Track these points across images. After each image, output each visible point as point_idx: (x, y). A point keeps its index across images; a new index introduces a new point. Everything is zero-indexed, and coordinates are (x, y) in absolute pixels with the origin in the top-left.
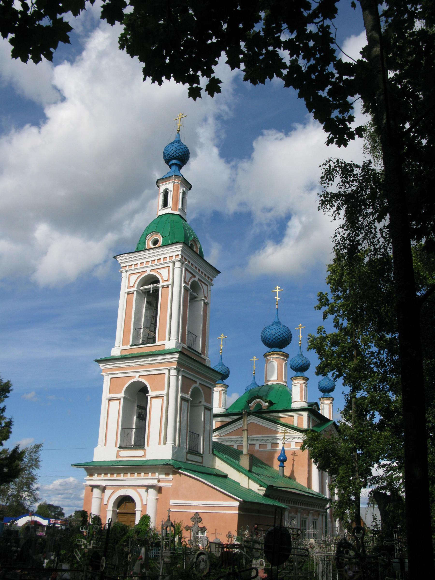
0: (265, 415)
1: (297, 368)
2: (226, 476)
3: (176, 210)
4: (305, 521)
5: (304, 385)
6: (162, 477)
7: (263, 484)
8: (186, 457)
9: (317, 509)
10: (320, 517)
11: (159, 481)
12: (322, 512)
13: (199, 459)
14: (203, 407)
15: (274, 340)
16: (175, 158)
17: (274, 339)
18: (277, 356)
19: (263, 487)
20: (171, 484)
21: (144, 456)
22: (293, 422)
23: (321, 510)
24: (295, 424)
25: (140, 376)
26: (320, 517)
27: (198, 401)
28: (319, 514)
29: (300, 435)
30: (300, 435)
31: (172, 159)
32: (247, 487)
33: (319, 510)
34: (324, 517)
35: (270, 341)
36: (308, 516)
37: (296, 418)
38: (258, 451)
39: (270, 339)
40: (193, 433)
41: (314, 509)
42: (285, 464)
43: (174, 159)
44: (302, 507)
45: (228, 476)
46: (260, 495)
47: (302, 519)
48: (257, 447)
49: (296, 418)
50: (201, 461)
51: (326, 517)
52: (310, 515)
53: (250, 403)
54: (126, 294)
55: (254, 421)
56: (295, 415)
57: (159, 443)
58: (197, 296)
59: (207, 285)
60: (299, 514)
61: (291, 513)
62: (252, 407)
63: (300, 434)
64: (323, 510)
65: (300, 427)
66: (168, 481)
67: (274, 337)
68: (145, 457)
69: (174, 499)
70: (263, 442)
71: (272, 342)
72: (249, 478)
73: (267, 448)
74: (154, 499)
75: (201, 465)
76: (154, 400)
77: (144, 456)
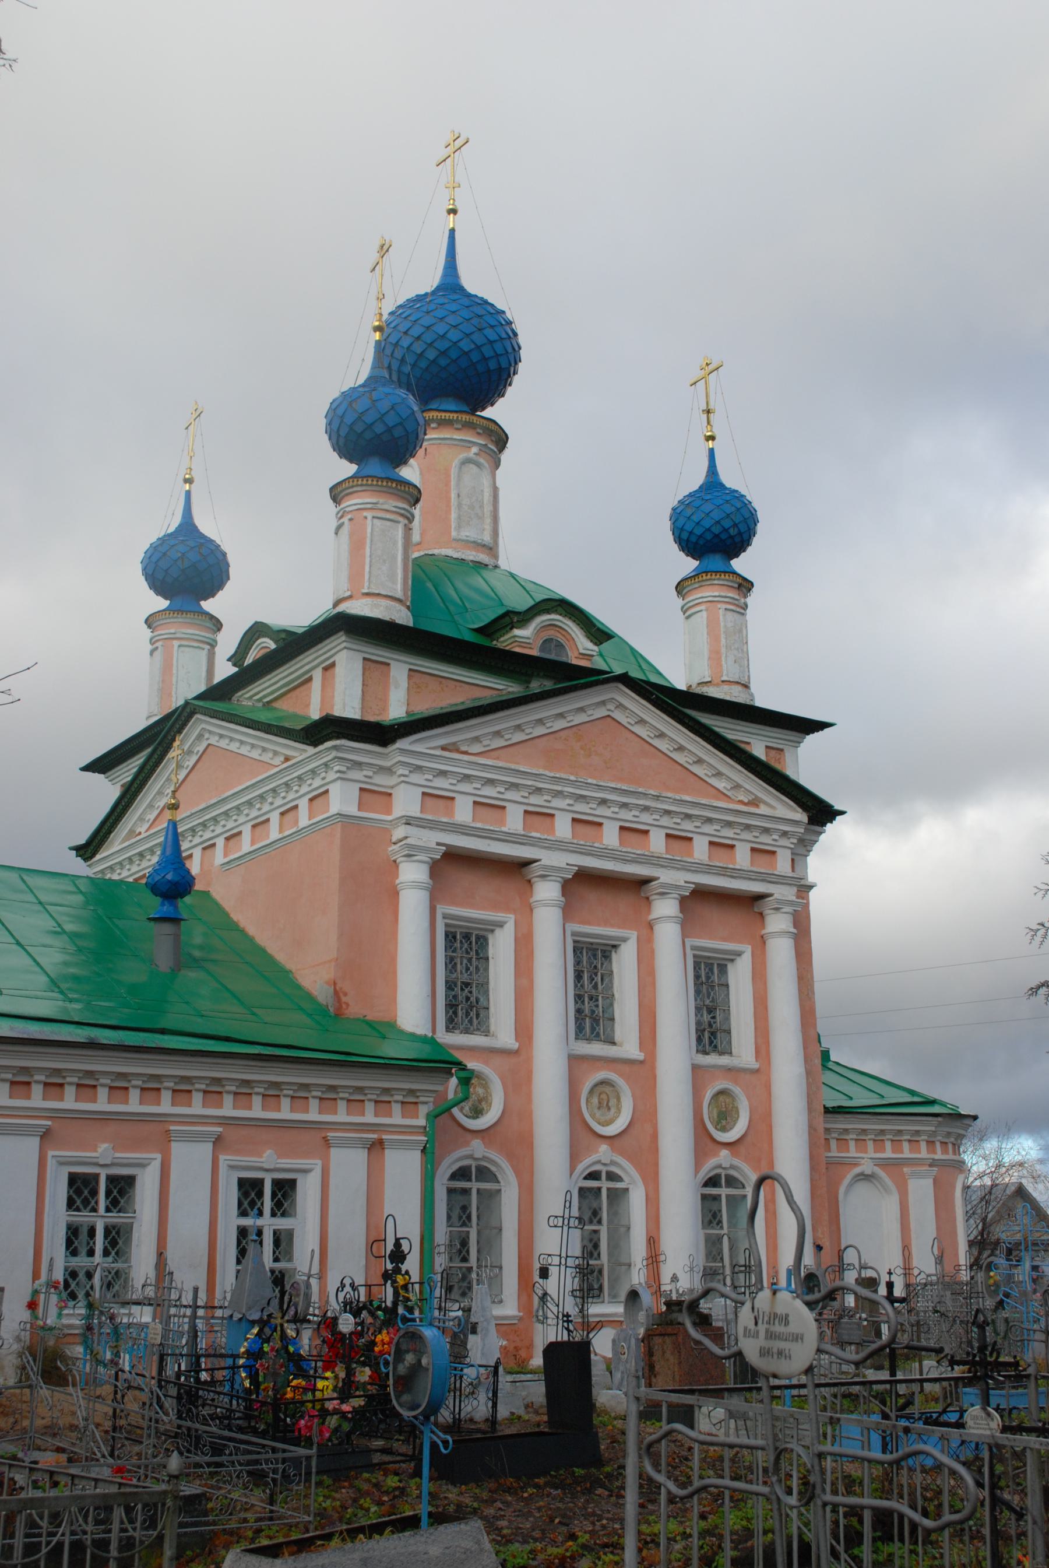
70: (442, 784)
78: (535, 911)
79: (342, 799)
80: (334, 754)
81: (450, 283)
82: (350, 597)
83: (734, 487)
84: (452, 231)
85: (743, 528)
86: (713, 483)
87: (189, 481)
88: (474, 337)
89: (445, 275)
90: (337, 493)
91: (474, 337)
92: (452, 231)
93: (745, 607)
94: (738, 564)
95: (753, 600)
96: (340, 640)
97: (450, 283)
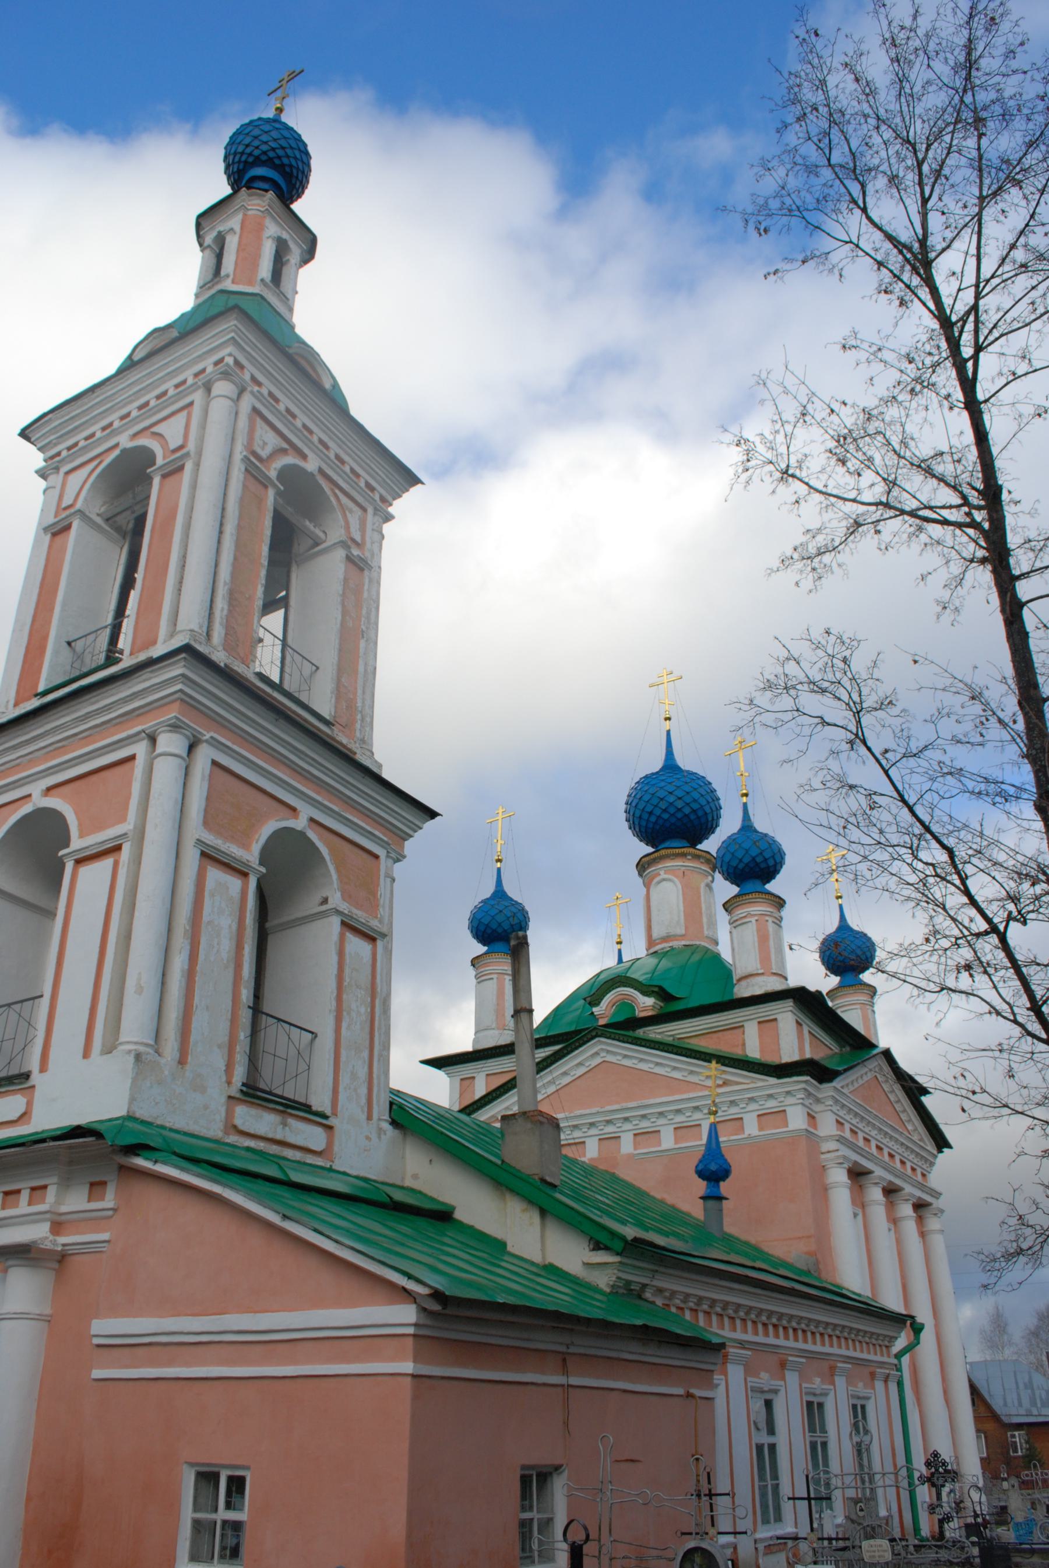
0: (640, 1033)
1: (741, 866)
2: (443, 1216)
3: (250, 283)
4: (821, 1405)
5: (770, 920)
6: (76, 1201)
7: (603, 1238)
8: (229, 1114)
9: (865, 1356)
10: (879, 1385)
11: (57, 1227)
12: (882, 1364)
13: (311, 1136)
14: (335, 921)
15: (666, 816)
16: (269, 163)
17: (665, 811)
18: (678, 862)
19: (607, 1248)
20: (105, 1236)
21: (24, 1117)
22: (744, 1044)
23: (878, 1358)
24: (753, 1051)
25: (49, 790)
26: (879, 1385)
27: (317, 898)
28: (873, 1375)
29: (772, 1086)
30: (772, 1086)
31: (258, 162)
32: (537, 1258)
33: (871, 1357)
34: (893, 1387)
35: (653, 819)
36: (833, 1383)
37: (752, 1030)
38: (630, 1156)
39: (651, 813)
40: (279, 1020)
41: (851, 1353)
42: (725, 1187)
43: (264, 164)
44: (801, 1345)
45: (458, 1215)
46: (596, 1289)
47: (806, 1398)
48: (627, 1145)
49: (752, 1030)
50: (319, 1144)
51: (900, 1384)
52: (840, 1381)
53: (597, 1004)
54: (49, 536)
55: (610, 1058)
56: (750, 1021)
57: (86, 1054)
58: (321, 535)
59: (365, 510)
60: (792, 1378)
61: (756, 1375)
62: (602, 1016)
63: (773, 1081)
64: (885, 1359)
65: (772, 1059)
66: (93, 1220)
67: (663, 805)
68: (28, 1122)
69: (114, 1311)
70: (645, 1124)
71: (661, 822)
72: (543, 1213)
73: (660, 1145)
74: (39, 1318)
75: (319, 1162)
76: (85, 871)
77: (24, 1117)
78: (830, 1191)
79: (797, 1120)
80: (803, 1085)
81: (670, 766)
82: (762, 974)
83: (765, 832)
84: (668, 732)
85: (771, 863)
86: (500, 893)
87: (619, 943)
88: (676, 793)
89: (666, 760)
90: (475, 962)
91: (676, 793)
92: (668, 732)
93: (781, 919)
94: (772, 887)
95: (785, 912)
96: (789, 1004)
97: (670, 766)
